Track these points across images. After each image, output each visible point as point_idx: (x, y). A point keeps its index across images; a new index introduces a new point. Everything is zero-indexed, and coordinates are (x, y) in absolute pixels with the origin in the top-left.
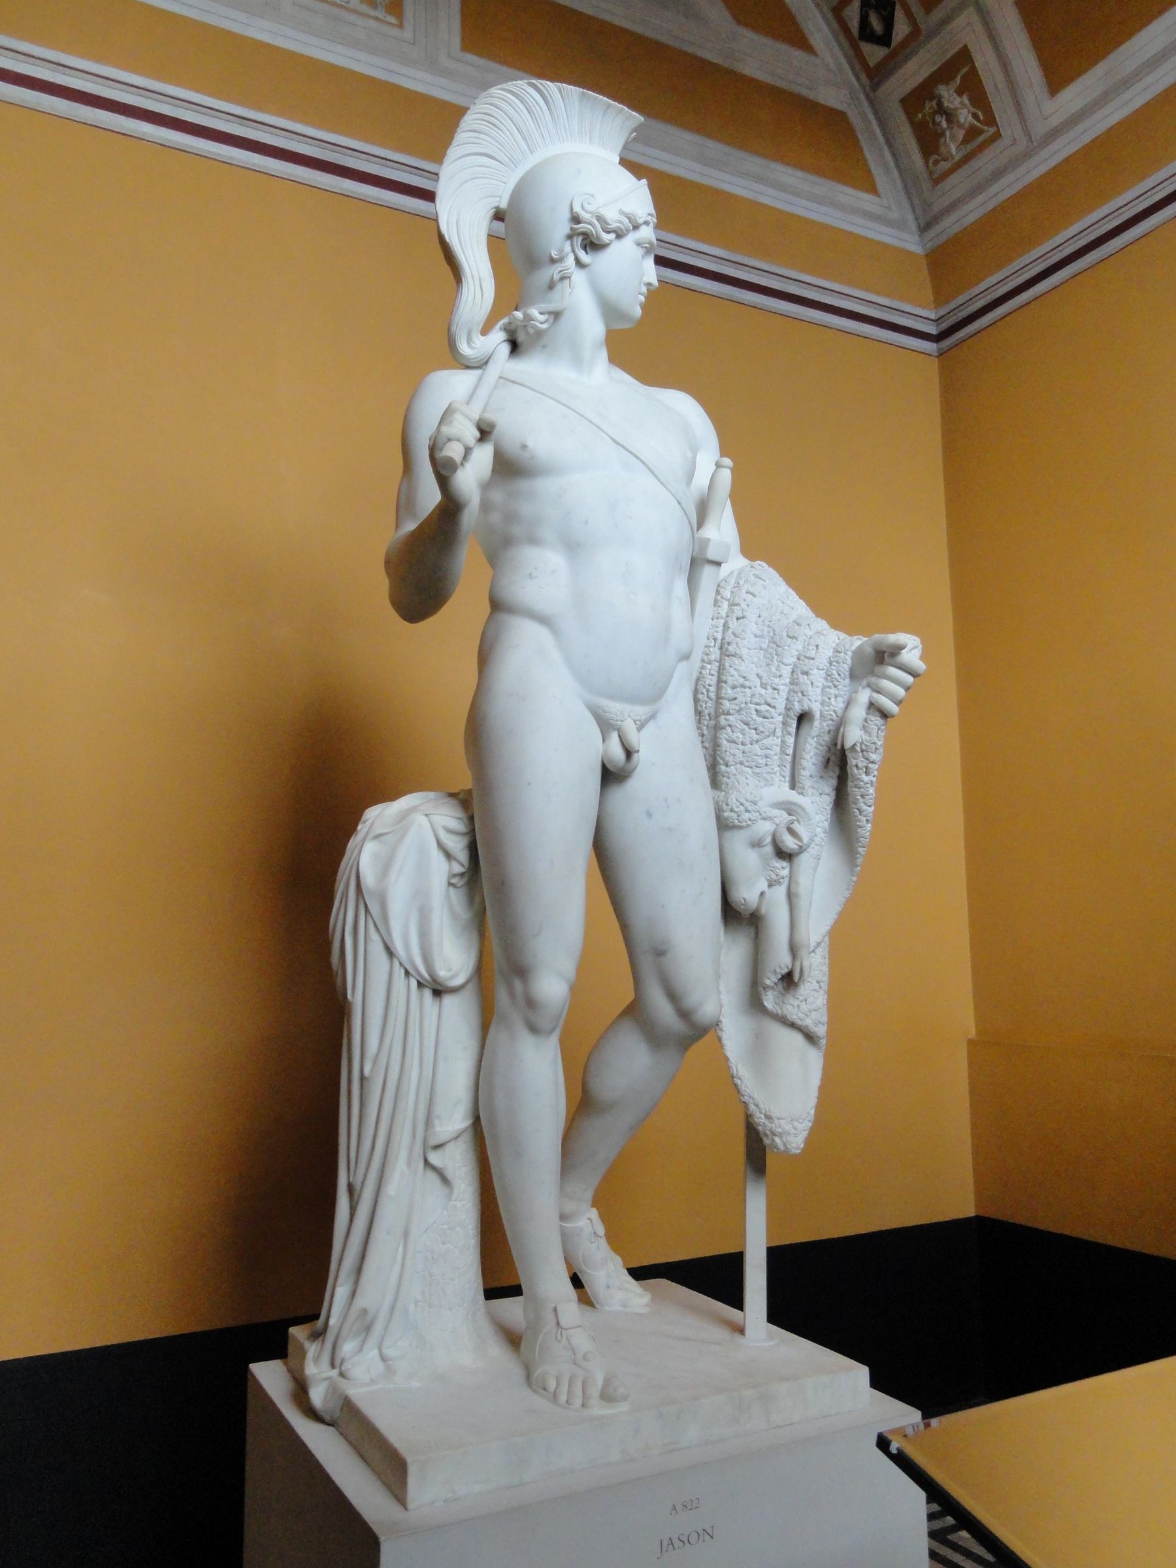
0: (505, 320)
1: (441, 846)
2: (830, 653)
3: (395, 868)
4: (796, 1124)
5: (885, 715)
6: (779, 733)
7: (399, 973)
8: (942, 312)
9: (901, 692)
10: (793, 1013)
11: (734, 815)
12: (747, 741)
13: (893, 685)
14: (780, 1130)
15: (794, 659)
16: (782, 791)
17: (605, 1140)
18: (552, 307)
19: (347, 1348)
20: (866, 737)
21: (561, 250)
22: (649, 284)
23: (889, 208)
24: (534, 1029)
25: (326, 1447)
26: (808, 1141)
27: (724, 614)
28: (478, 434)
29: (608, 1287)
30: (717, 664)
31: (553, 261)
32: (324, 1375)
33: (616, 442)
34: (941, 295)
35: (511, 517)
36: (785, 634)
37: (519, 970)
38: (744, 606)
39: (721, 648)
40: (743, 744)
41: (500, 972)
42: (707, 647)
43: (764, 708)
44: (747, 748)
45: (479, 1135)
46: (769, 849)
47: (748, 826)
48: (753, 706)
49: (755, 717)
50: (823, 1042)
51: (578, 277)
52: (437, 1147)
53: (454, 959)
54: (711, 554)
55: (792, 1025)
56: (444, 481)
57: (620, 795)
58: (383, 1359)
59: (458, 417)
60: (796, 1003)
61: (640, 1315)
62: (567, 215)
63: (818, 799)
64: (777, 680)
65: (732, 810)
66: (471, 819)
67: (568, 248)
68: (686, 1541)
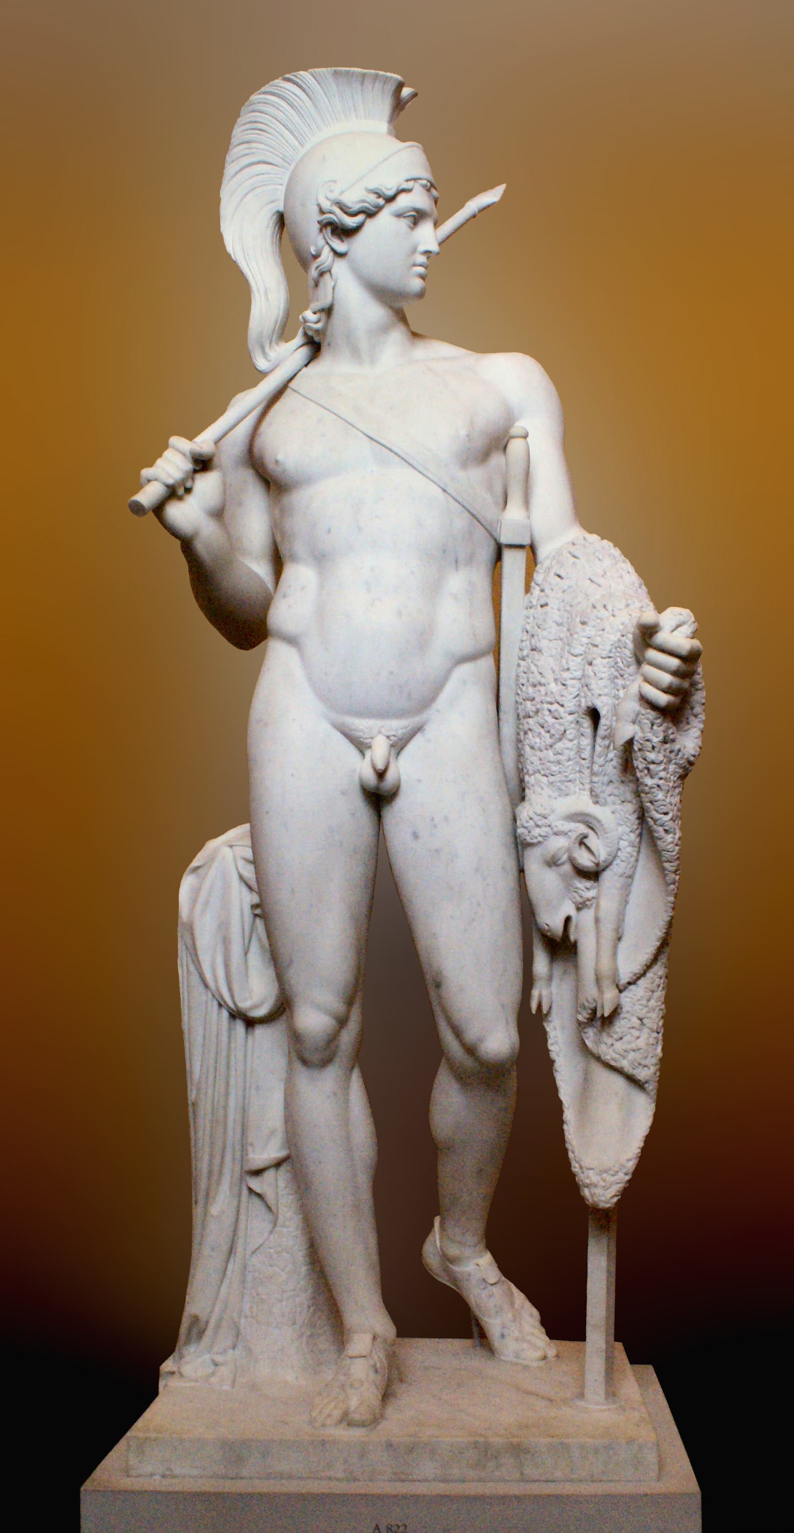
1: (241, 877)
10: (608, 1054)
11: (526, 832)
14: (587, 1181)
18: (324, 302)
22: (427, 253)
29: (503, 1336)
33: (371, 439)
36: (578, 619)
43: (556, 706)
46: (567, 868)
47: (539, 842)
48: (546, 706)
50: (652, 1087)
52: (258, 1173)
60: (610, 1041)
61: (526, 1367)
62: (316, 209)
63: (618, 807)
67: (321, 242)
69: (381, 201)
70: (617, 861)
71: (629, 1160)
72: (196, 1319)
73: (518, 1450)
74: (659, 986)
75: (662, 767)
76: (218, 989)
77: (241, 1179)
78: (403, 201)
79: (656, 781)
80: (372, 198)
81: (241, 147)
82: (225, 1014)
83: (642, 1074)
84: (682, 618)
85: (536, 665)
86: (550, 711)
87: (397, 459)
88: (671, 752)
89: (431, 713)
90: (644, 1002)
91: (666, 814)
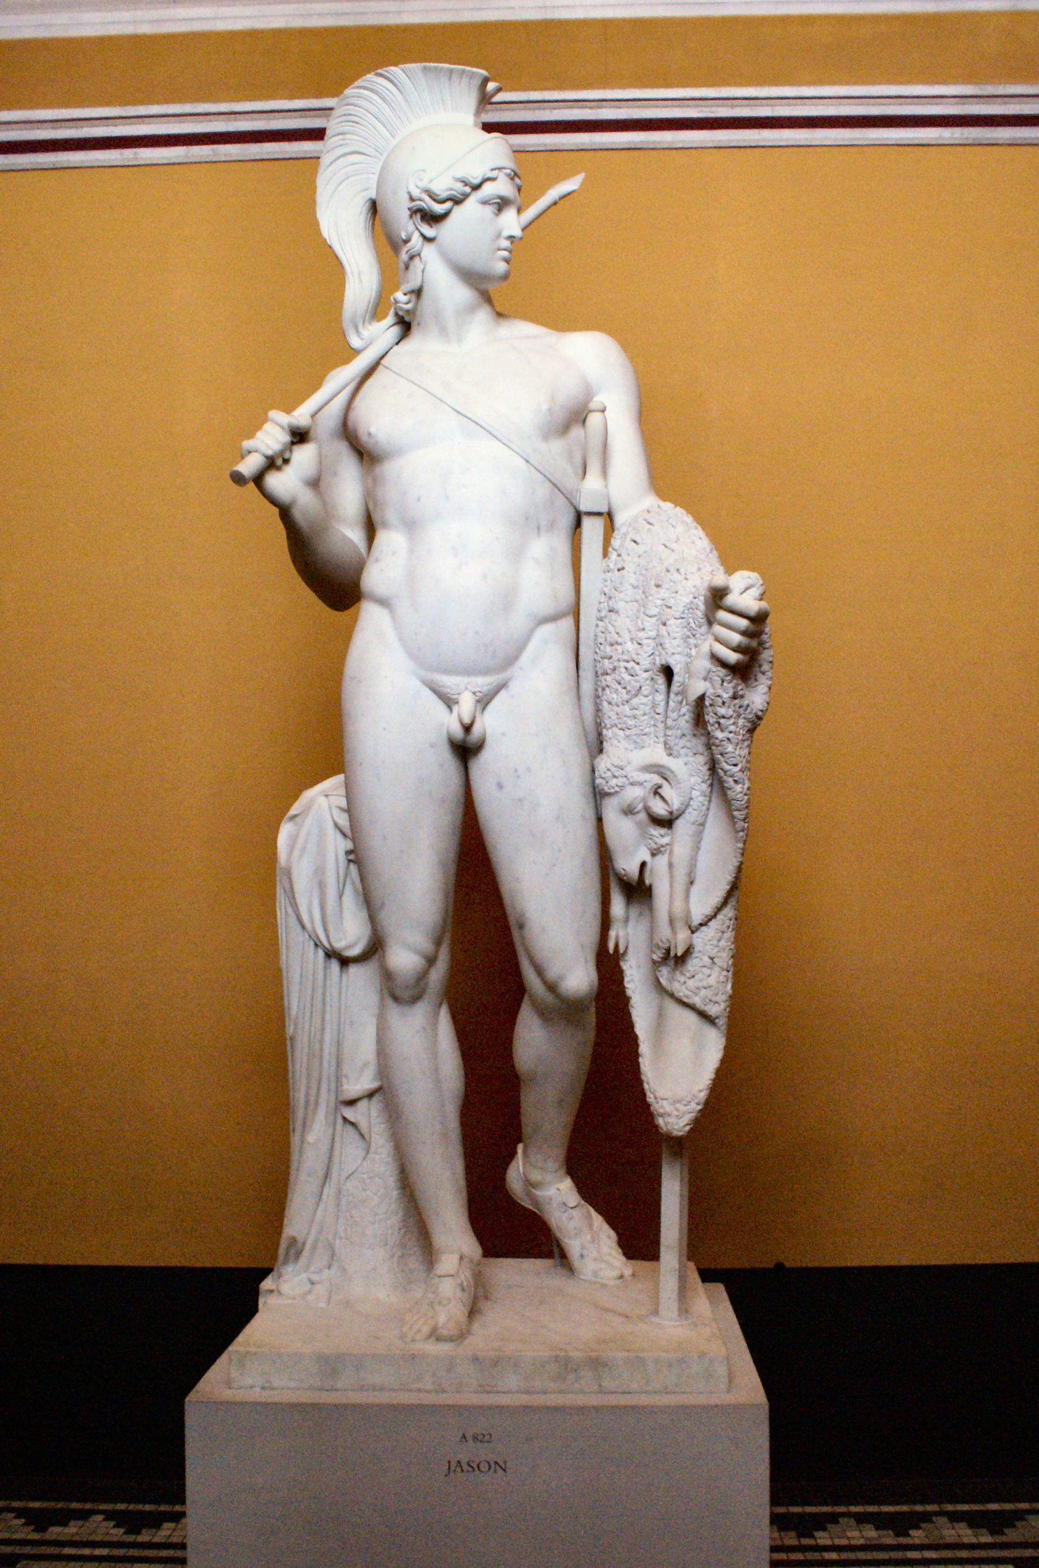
4: (678, 1105)
9: (736, 638)
10: (681, 992)
14: (661, 1111)
29: (582, 1256)
36: (653, 582)
43: (632, 664)
46: (643, 816)
47: (616, 792)
48: (622, 664)
50: (721, 1022)
52: (351, 1103)
60: (682, 979)
62: (407, 197)
63: (691, 759)
67: (411, 227)
68: (474, 1467)
69: (468, 189)
71: (700, 1091)
72: (293, 1241)
73: (597, 1364)
74: (729, 927)
75: (732, 721)
77: (336, 1109)
78: (488, 189)
79: (726, 734)
80: (460, 187)
82: (321, 953)
83: (713, 1010)
84: (750, 582)
85: (613, 626)
88: (740, 707)
89: (514, 671)
90: (715, 942)
91: (735, 765)
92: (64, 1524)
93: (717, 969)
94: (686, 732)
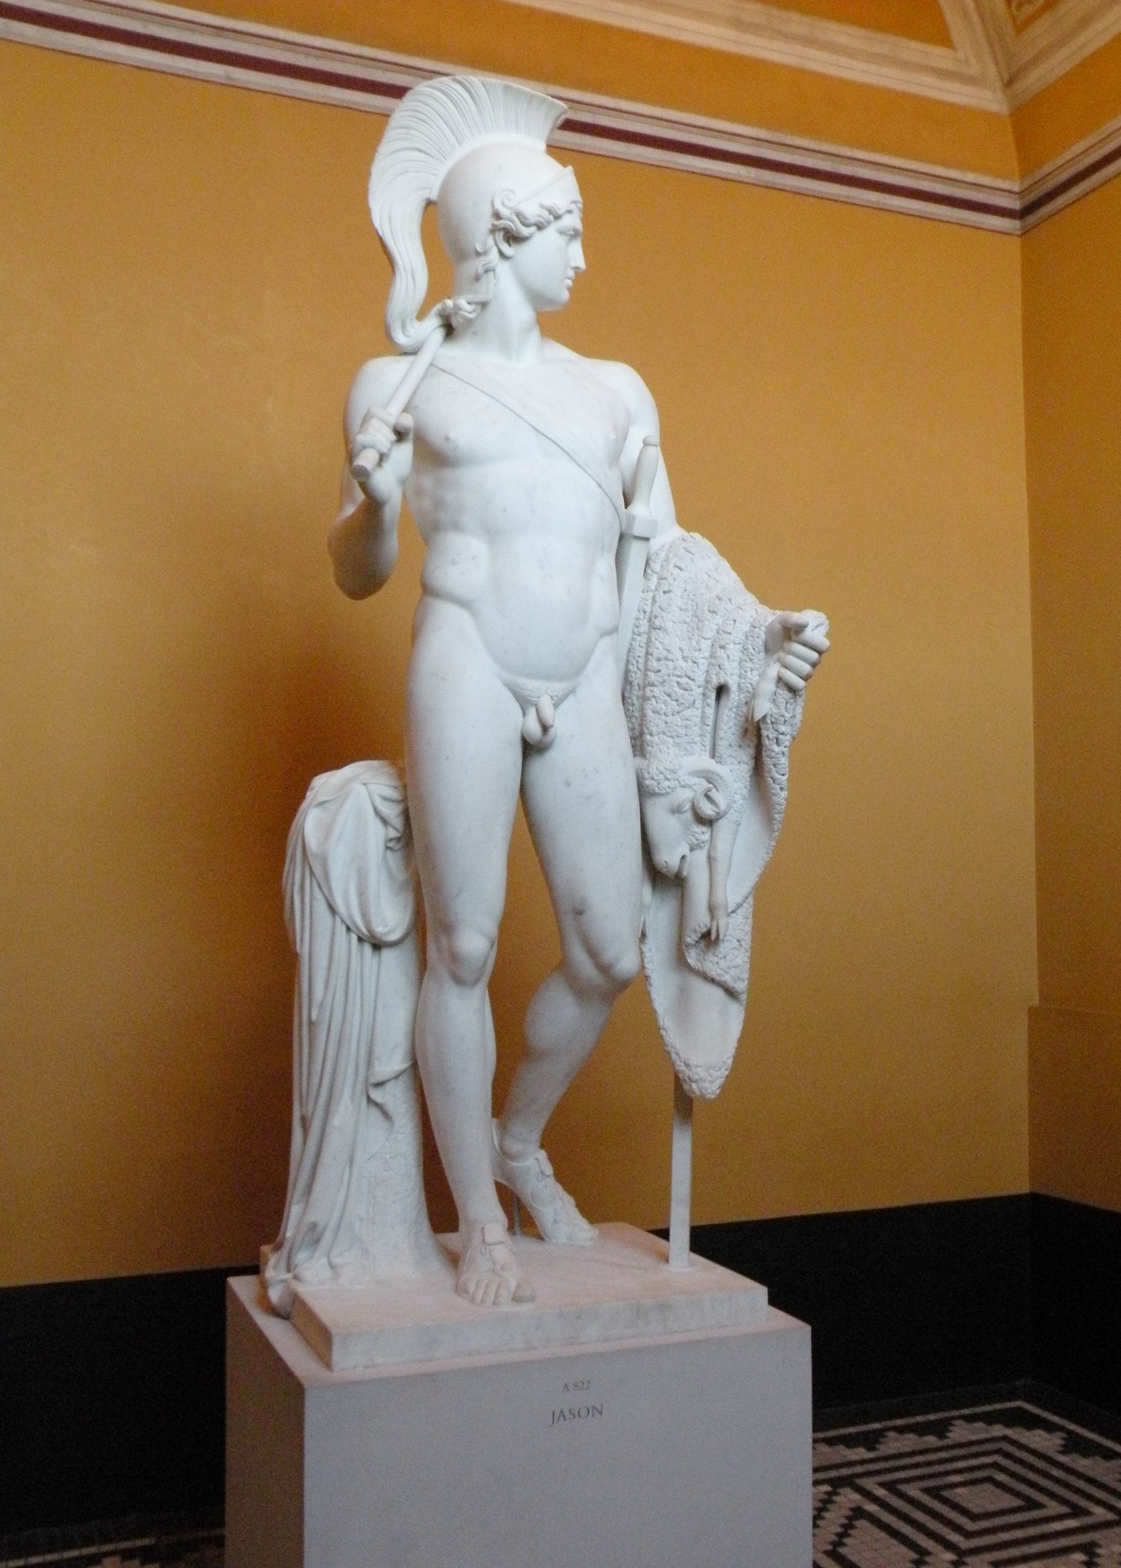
0: (439, 306)
1: (377, 812)
2: (747, 628)
3: (336, 832)
5: (793, 690)
6: (698, 704)
7: (341, 929)
8: (1029, 181)
9: (806, 668)
10: (713, 971)
12: (669, 711)
13: (799, 659)
14: (697, 1077)
15: (714, 633)
16: (705, 762)
17: (545, 1087)
19: (301, 1257)
20: (775, 710)
21: (484, 245)
22: (576, 268)
23: (966, 62)
24: (458, 980)
25: (276, 1332)
26: (724, 1087)
27: (653, 587)
28: (393, 437)
29: (555, 1222)
30: (646, 636)
31: (478, 254)
32: (280, 1277)
33: (536, 430)
34: (1027, 165)
35: (439, 504)
36: (706, 608)
37: (447, 928)
38: (670, 580)
39: (650, 620)
40: (665, 715)
41: (428, 926)
42: (637, 619)
43: (684, 680)
44: (670, 719)
45: (417, 1076)
46: (689, 815)
48: (675, 679)
49: (676, 689)
50: (744, 997)
51: (503, 268)
52: (379, 1085)
53: (391, 917)
54: (637, 531)
55: (712, 981)
56: (364, 487)
57: (539, 766)
58: (332, 1266)
59: (374, 423)
60: (715, 960)
61: (583, 1247)
64: (696, 654)
65: (652, 779)
66: (405, 787)
68: (576, 1414)
69: (551, 218)
70: (732, 811)
76: (350, 916)
81: (398, 131)
84: (821, 620)
86: (678, 683)
87: (561, 452)
92: (1086, 1455)
93: (742, 950)
94: (733, 743)
